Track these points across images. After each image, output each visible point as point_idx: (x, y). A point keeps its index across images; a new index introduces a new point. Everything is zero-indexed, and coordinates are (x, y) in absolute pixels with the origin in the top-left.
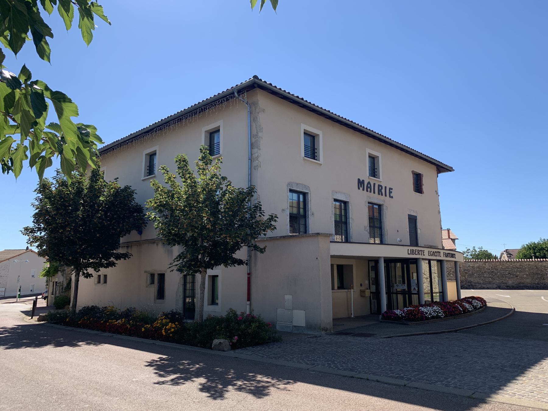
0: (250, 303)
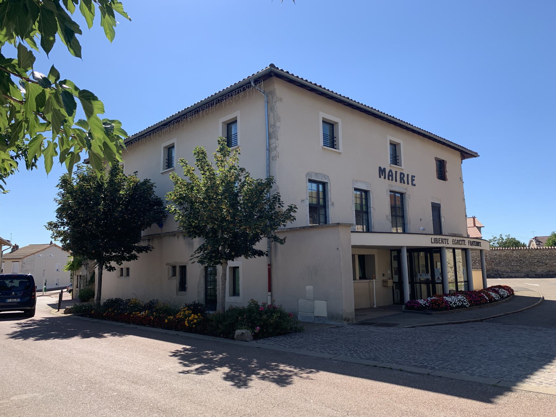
0: (271, 294)
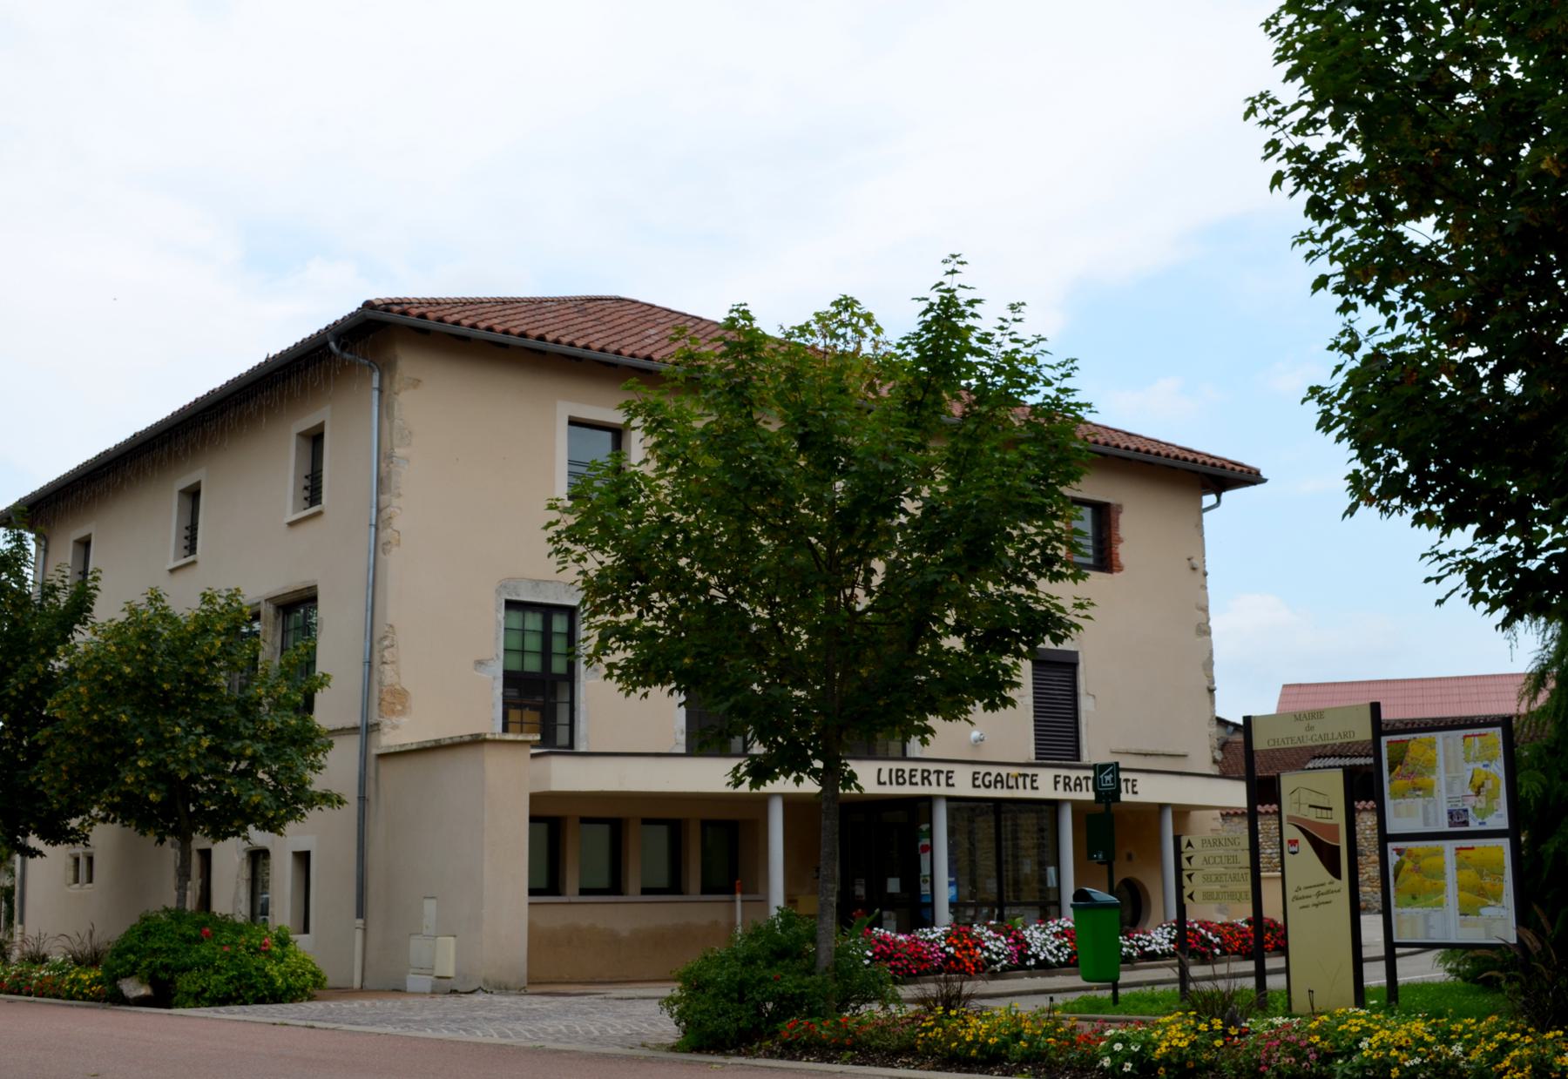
0: (365, 924)
